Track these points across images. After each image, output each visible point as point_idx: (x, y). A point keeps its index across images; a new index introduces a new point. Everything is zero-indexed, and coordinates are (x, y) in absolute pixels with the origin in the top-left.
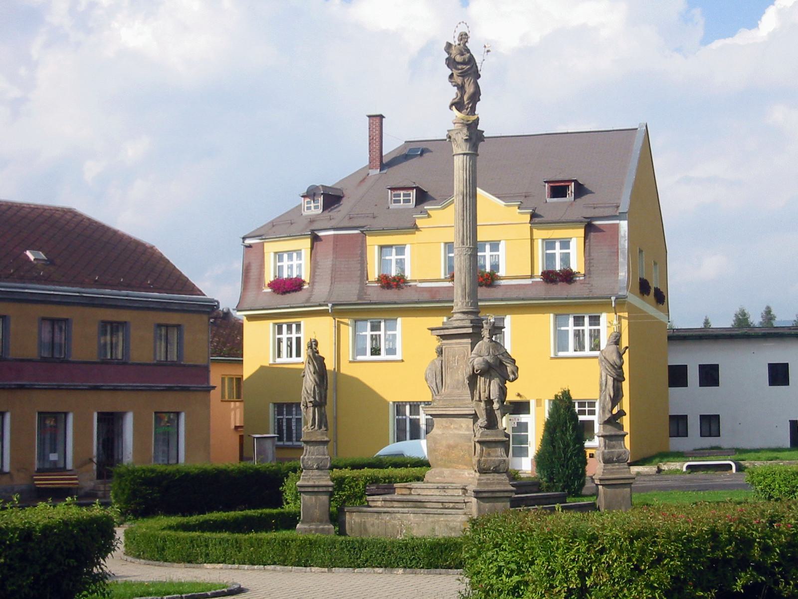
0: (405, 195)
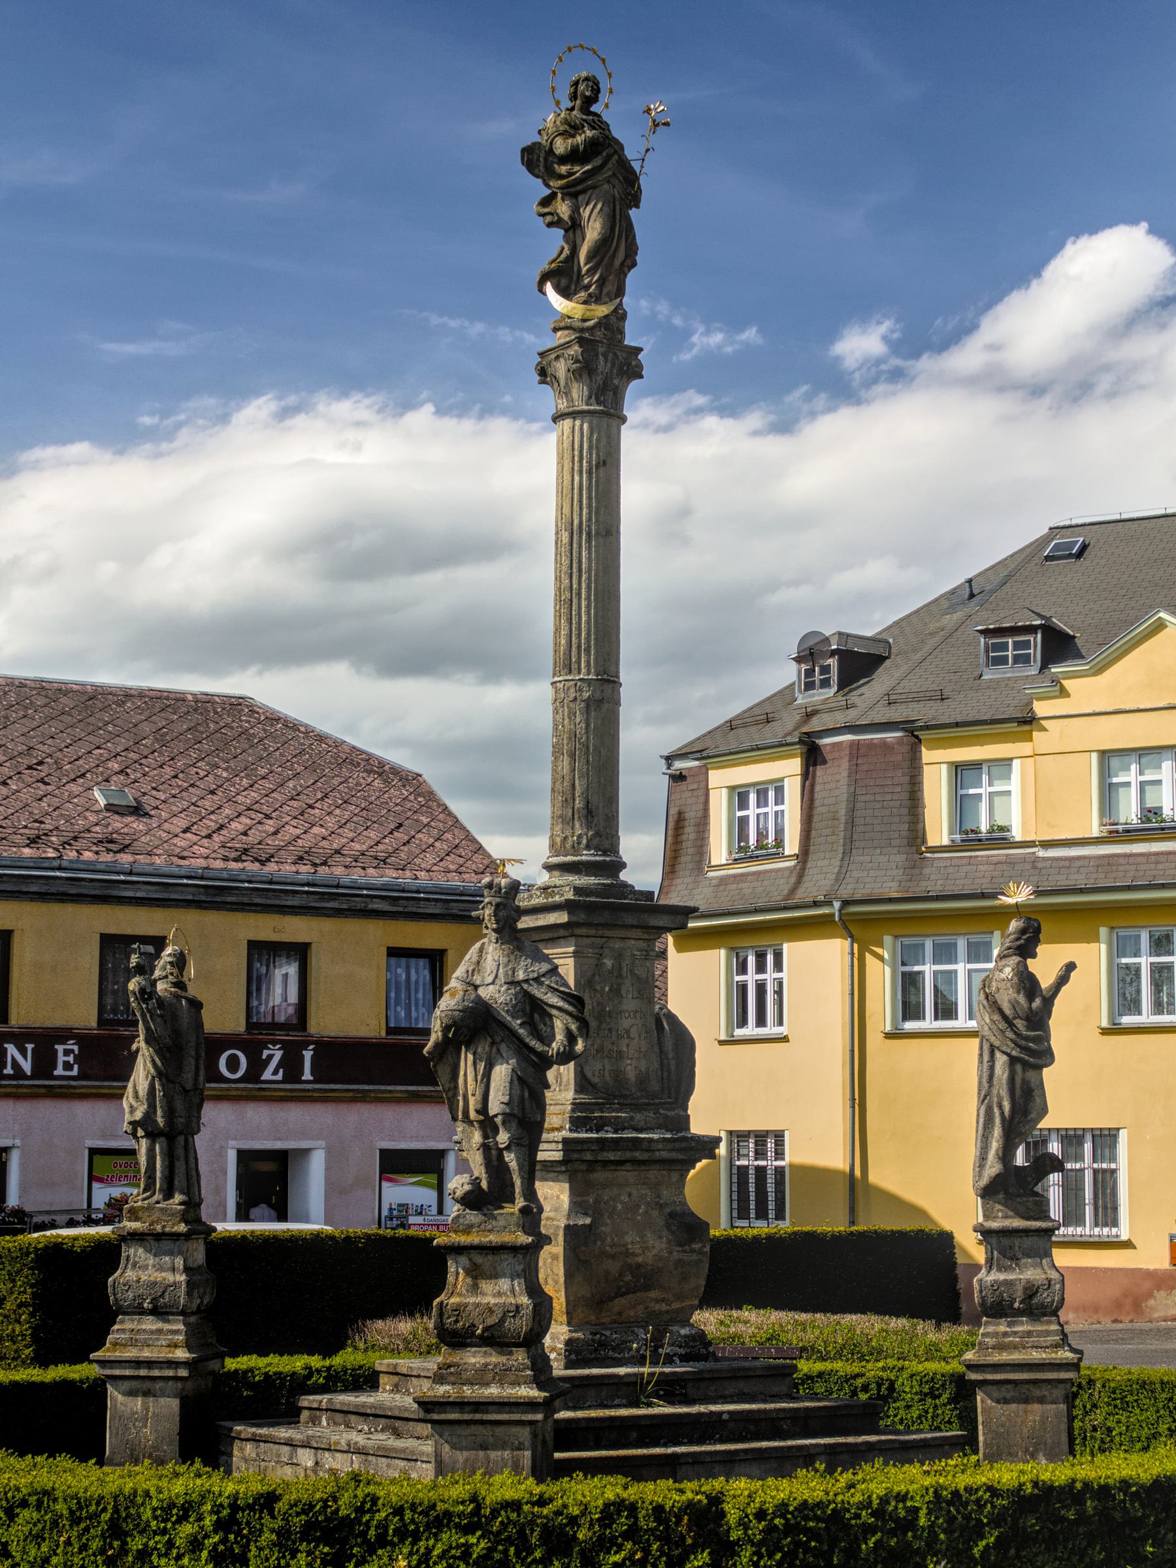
0: (1017, 645)
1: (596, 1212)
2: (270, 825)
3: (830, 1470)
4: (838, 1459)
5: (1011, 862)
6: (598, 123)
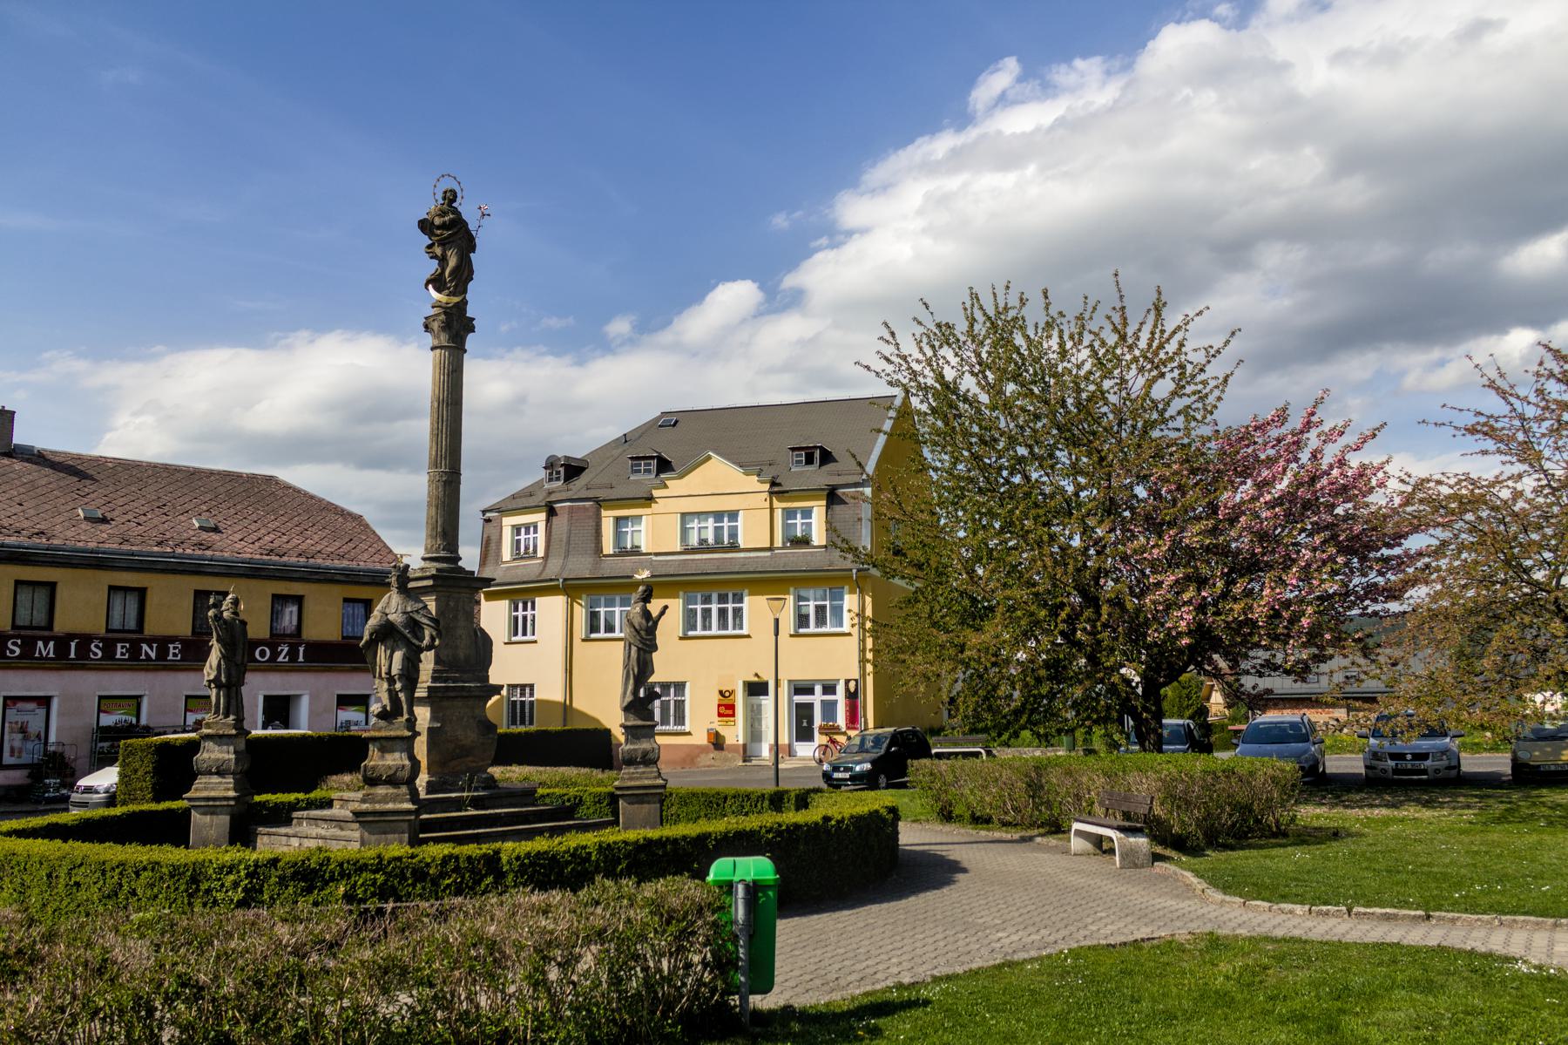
1: (443, 721)
2: (285, 539)
3: (551, 836)
4: (554, 832)
5: (641, 562)
6: (456, 211)
